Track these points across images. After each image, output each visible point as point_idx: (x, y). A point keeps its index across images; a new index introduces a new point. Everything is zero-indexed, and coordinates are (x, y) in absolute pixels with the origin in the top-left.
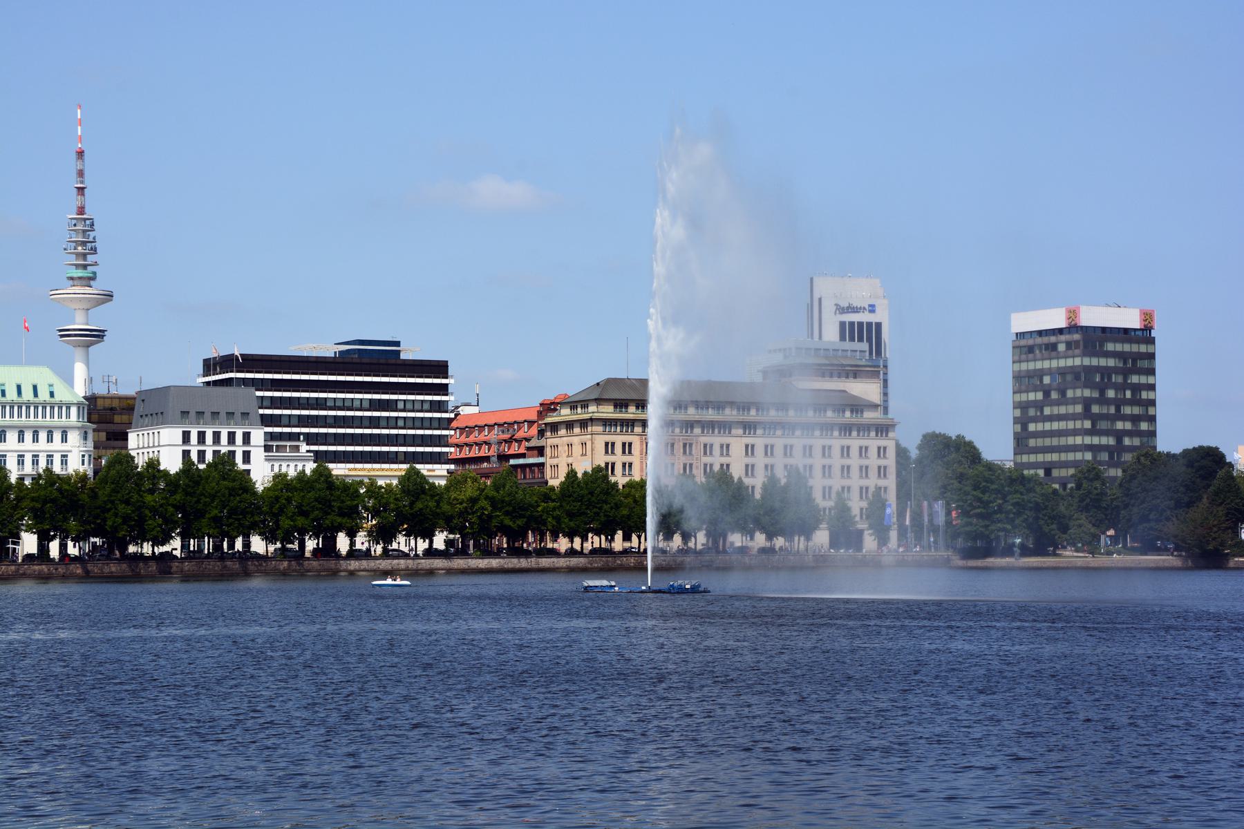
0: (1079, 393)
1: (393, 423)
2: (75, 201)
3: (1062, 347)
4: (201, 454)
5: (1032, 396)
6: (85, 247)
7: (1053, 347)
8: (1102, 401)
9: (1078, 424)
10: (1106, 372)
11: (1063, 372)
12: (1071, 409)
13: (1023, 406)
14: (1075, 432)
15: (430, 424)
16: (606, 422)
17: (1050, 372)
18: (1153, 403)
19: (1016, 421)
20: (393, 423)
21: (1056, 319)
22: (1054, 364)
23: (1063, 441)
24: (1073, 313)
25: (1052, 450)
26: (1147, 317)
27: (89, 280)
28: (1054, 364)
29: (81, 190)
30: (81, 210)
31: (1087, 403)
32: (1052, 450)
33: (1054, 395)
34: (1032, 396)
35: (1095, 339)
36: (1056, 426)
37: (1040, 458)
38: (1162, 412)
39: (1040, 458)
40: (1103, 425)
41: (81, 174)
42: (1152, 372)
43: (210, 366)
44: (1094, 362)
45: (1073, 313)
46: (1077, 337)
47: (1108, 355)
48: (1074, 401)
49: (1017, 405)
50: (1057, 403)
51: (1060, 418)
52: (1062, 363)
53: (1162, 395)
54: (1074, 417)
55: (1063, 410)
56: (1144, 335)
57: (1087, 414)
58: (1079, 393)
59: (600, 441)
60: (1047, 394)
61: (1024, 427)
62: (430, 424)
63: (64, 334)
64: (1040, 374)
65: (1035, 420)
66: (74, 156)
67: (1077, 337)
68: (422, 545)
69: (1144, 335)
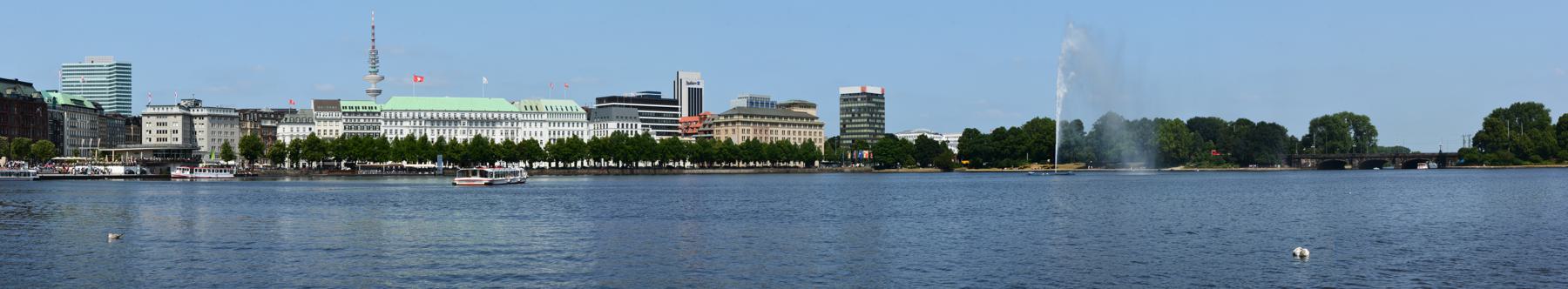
0: (866, 115)
1: (662, 121)
2: (371, 44)
3: (859, 100)
4: (800, 139)
5: (847, 116)
6: (375, 61)
7: (856, 99)
8: (872, 118)
9: (865, 125)
10: (873, 108)
11: (859, 108)
12: (862, 120)
13: (844, 119)
14: (864, 128)
15: (672, 122)
16: (743, 122)
17: (855, 108)
18: (884, 119)
19: (841, 124)
20: (662, 121)
21: (858, 90)
22: (856, 105)
23: (859, 131)
24: (863, 88)
25: (855, 134)
26: (883, 90)
27: (376, 73)
28: (856, 105)
29: (373, 40)
30: (373, 47)
31: (868, 118)
32: (855, 134)
33: (856, 116)
34: (847, 116)
35: (870, 97)
36: (856, 126)
37: (850, 136)
38: (886, 122)
39: (850, 136)
40: (872, 126)
41: (373, 34)
42: (883, 109)
43: (599, 100)
44: (870, 105)
45: (863, 88)
46: (865, 96)
47: (873, 102)
48: (864, 118)
49: (841, 119)
50: (857, 118)
51: (858, 123)
52: (859, 105)
53: (886, 117)
54: (864, 123)
55: (859, 121)
56: (881, 96)
57: (868, 122)
58: (866, 115)
59: (741, 128)
60: (853, 115)
61: (844, 126)
62: (672, 122)
63: (368, 92)
64: (851, 108)
65: (849, 124)
66: (371, 28)
67: (865, 96)
68: (650, 164)
69: (881, 96)
